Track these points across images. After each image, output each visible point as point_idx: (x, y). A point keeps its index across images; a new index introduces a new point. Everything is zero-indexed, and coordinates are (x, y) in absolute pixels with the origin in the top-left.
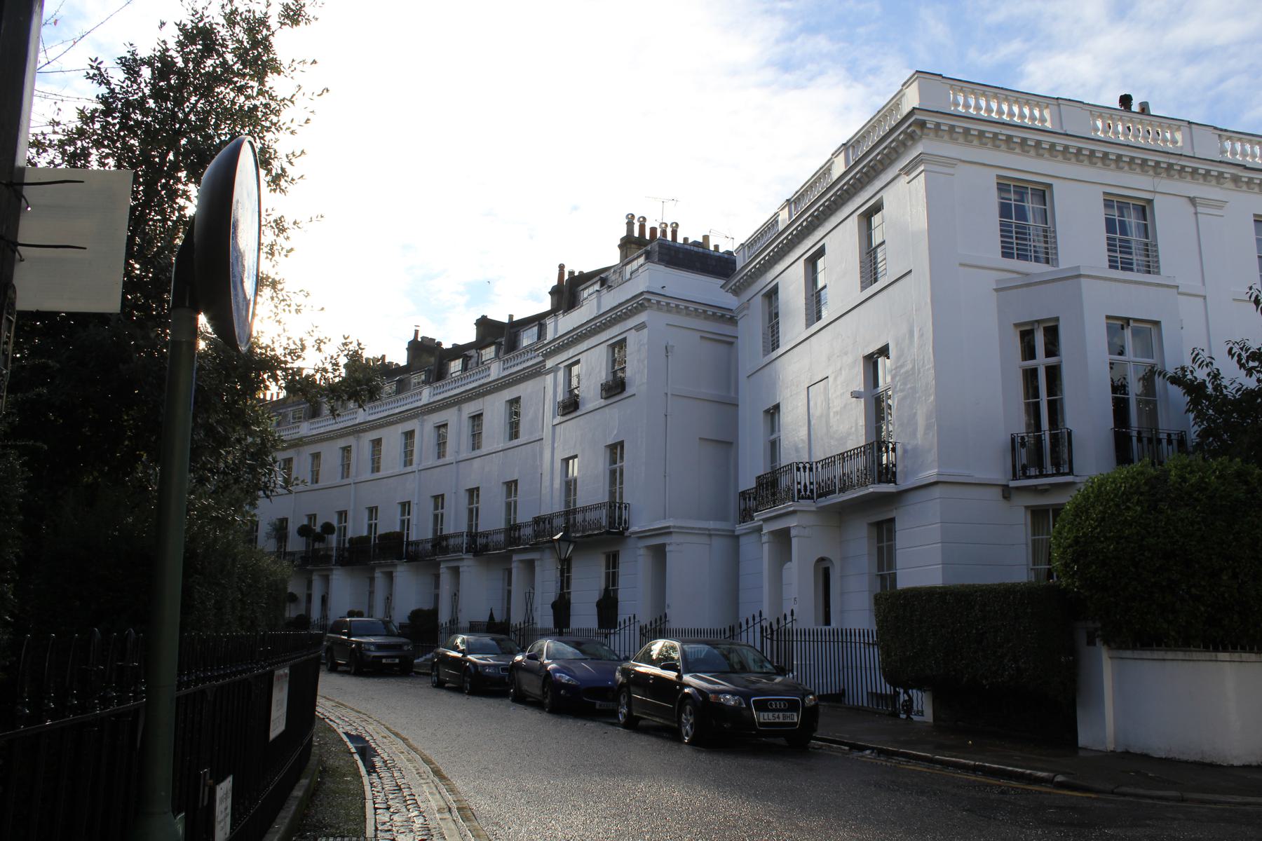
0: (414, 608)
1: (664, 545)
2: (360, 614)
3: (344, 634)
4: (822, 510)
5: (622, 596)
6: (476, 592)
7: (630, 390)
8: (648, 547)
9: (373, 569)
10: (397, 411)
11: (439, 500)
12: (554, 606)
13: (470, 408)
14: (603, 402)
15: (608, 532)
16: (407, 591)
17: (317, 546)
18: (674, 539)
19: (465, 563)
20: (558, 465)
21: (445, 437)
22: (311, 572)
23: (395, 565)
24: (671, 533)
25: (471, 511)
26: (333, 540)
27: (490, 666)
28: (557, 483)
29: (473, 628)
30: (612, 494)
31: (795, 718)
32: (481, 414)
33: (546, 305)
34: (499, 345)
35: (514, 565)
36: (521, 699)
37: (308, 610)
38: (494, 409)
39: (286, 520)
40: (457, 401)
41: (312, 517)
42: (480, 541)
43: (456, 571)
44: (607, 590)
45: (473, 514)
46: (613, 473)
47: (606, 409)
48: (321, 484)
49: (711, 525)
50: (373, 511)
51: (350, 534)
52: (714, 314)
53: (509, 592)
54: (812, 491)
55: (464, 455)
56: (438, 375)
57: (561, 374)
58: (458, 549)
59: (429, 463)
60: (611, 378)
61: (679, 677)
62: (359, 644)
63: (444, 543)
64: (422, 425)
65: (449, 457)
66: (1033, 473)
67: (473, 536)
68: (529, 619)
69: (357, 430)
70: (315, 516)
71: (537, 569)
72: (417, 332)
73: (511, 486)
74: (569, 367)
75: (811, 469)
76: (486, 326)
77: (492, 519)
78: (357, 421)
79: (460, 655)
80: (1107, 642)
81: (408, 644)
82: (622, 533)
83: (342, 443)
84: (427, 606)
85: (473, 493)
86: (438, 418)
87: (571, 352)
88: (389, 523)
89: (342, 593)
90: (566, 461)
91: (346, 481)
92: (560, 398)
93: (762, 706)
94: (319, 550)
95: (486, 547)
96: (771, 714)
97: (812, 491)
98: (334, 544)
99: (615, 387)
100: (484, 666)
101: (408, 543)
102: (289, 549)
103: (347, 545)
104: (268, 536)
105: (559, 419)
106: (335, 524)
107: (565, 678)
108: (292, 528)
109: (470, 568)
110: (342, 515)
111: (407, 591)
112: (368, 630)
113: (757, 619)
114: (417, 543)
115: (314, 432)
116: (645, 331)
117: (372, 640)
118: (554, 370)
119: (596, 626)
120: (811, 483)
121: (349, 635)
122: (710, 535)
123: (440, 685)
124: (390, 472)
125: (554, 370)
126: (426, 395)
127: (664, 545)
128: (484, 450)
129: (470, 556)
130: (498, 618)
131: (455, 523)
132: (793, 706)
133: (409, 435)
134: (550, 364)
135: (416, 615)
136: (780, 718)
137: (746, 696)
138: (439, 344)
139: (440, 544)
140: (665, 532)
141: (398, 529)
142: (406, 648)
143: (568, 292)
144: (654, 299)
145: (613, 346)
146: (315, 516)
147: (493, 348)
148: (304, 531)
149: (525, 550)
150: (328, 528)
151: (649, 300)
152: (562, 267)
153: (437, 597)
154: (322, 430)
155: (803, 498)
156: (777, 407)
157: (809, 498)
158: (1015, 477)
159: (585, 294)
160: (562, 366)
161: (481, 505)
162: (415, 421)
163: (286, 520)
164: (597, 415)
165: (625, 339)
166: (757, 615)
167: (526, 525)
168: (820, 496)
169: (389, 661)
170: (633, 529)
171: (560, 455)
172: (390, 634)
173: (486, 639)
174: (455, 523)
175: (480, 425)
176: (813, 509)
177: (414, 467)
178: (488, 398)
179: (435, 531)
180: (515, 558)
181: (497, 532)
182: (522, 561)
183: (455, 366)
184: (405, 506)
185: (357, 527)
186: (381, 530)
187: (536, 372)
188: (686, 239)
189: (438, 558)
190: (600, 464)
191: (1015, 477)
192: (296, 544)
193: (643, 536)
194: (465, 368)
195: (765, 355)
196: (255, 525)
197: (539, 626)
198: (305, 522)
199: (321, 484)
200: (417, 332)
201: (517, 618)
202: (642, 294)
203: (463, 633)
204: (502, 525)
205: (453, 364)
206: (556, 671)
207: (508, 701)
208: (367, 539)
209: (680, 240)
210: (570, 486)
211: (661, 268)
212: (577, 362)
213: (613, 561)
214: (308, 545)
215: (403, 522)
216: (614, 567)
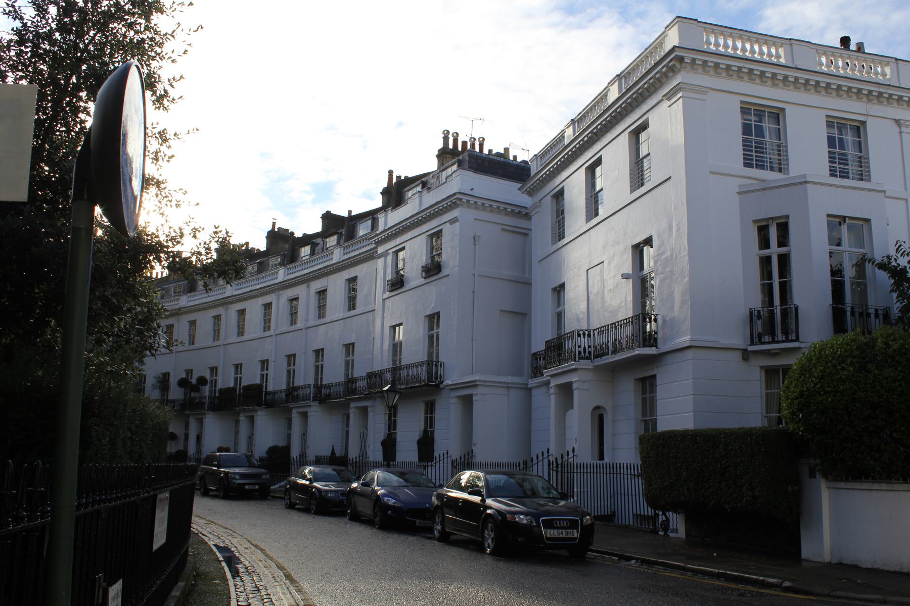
0: (271, 444)
1: (471, 396)
2: (227, 450)
3: (215, 466)
4: (598, 368)
5: (437, 436)
6: (321, 431)
7: (445, 272)
8: (458, 397)
9: (238, 414)
10: (258, 287)
11: (291, 358)
13: (317, 285)
14: (423, 281)
15: (427, 385)
16: (266, 432)
17: (193, 395)
18: (479, 390)
19: (312, 409)
20: (387, 331)
22: (188, 416)
23: (256, 411)
24: (477, 386)
25: (317, 367)
26: (206, 390)
27: (331, 491)
28: (387, 345)
29: (318, 461)
30: (430, 354)
31: (576, 534)
32: (326, 290)
33: (378, 203)
34: (340, 235)
35: (351, 411)
36: (356, 518)
37: (186, 445)
38: (336, 285)
39: (169, 374)
41: (189, 372)
42: (325, 391)
43: (305, 416)
44: (425, 431)
48: (196, 346)
49: (509, 379)
50: (238, 367)
51: (220, 386)
52: (513, 211)
53: (347, 432)
54: (590, 353)
55: (312, 322)
56: (291, 258)
57: (390, 258)
58: (306, 398)
60: (429, 261)
61: (483, 501)
62: (226, 474)
63: (296, 393)
64: (278, 299)
65: (300, 324)
66: (780, 339)
67: (318, 387)
68: (363, 454)
69: (225, 302)
70: (191, 371)
71: (370, 414)
72: (274, 224)
73: (350, 348)
74: (396, 253)
75: (589, 336)
76: (328, 217)
77: (334, 374)
79: (308, 483)
80: (826, 476)
81: (266, 474)
82: (437, 386)
83: (214, 312)
84: (281, 443)
85: (319, 353)
87: (398, 240)
88: (251, 377)
89: (214, 433)
90: (393, 328)
91: (216, 343)
92: (389, 277)
93: (549, 525)
94: (194, 398)
95: (329, 396)
96: (556, 531)
97: (590, 353)
98: (207, 394)
99: (433, 269)
100: (327, 491)
102: (170, 398)
103: (217, 394)
104: (154, 387)
105: (388, 294)
106: (208, 377)
107: (391, 501)
108: (173, 381)
109: (316, 413)
110: (214, 370)
111: (266, 432)
112: (234, 463)
113: (546, 455)
114: (274, 393)
115: (191, 304)
116: (458, 224)
117: (237, 470)
118: (385, 254)
120: (589, 347)
121: (219, 466)
122: (508, 388)
123: (291, 506)
124: (252, 336)
125: (385, 254)
126: (282, 275)
127: (471, 396)
130: (338, 453)
132: (573, 525)
133: (268, 306)
134: (381, 250)
135: (273, 450)
136: (563, 534)
137: (536, 516)
138: (292, 233)
139: (292, 393)
140: (473, 385)
141: (258, 382)
142: (264, 477)
143: (396, 192)
144: (465, 198)
145: (431, 236)
146: (191, 371)
147: (335, 237)
148: (183, 383)
150: (202, 381)
151: (461, 199)
152: (391, 172)
153: (289, 436)
154: (198, 302)
155: (582, 358)
156: (562, 286)
157: (587, 358)
158: (752, 343)
159: (410, 194)
160: (390, 251)
161: (325, 363)
162: (273, 295)
163: (169, 374)
165: (441, 231)
166: (545, 452)
167: (361, 379)
168: (596, 357)
169: (251, 487)
170: (448, 382)
172: (252, 466)
173: (329, 470)
174: (304, 377)
175: (325, 299)
176: (591, 367)
177: (272, 332)
179: (288, 383)
180: (352, 405)
181: (337, 384)
184: (265, 364)
185: (225, 380)
186: (245, 383)
187: (370, 256)
188: (490, 151)
189: (291, 405)
190: (421, 330)
191: (752, 343)
192: (176, 393)
193: (455, 388)
194: (313, 253)
195: (553, 244)
196: (143, 378)
197: (371, 459)
198: (184, 376)
199: (196, 346)
200: (274, 224)
201: (353, 454)
202: (455, 194)
203: (310, 465)
204: (342, 379)
205: (303, 249)
206: (384, 495)
207: (346, 519)
208: (233, 390)
209: (486, 151)
210: (396, 348)
211: (471, 174)
212: (403, 249)
213: (430, 408)
214: (185, 394)
215: (262, 376)
216: (431, 413)
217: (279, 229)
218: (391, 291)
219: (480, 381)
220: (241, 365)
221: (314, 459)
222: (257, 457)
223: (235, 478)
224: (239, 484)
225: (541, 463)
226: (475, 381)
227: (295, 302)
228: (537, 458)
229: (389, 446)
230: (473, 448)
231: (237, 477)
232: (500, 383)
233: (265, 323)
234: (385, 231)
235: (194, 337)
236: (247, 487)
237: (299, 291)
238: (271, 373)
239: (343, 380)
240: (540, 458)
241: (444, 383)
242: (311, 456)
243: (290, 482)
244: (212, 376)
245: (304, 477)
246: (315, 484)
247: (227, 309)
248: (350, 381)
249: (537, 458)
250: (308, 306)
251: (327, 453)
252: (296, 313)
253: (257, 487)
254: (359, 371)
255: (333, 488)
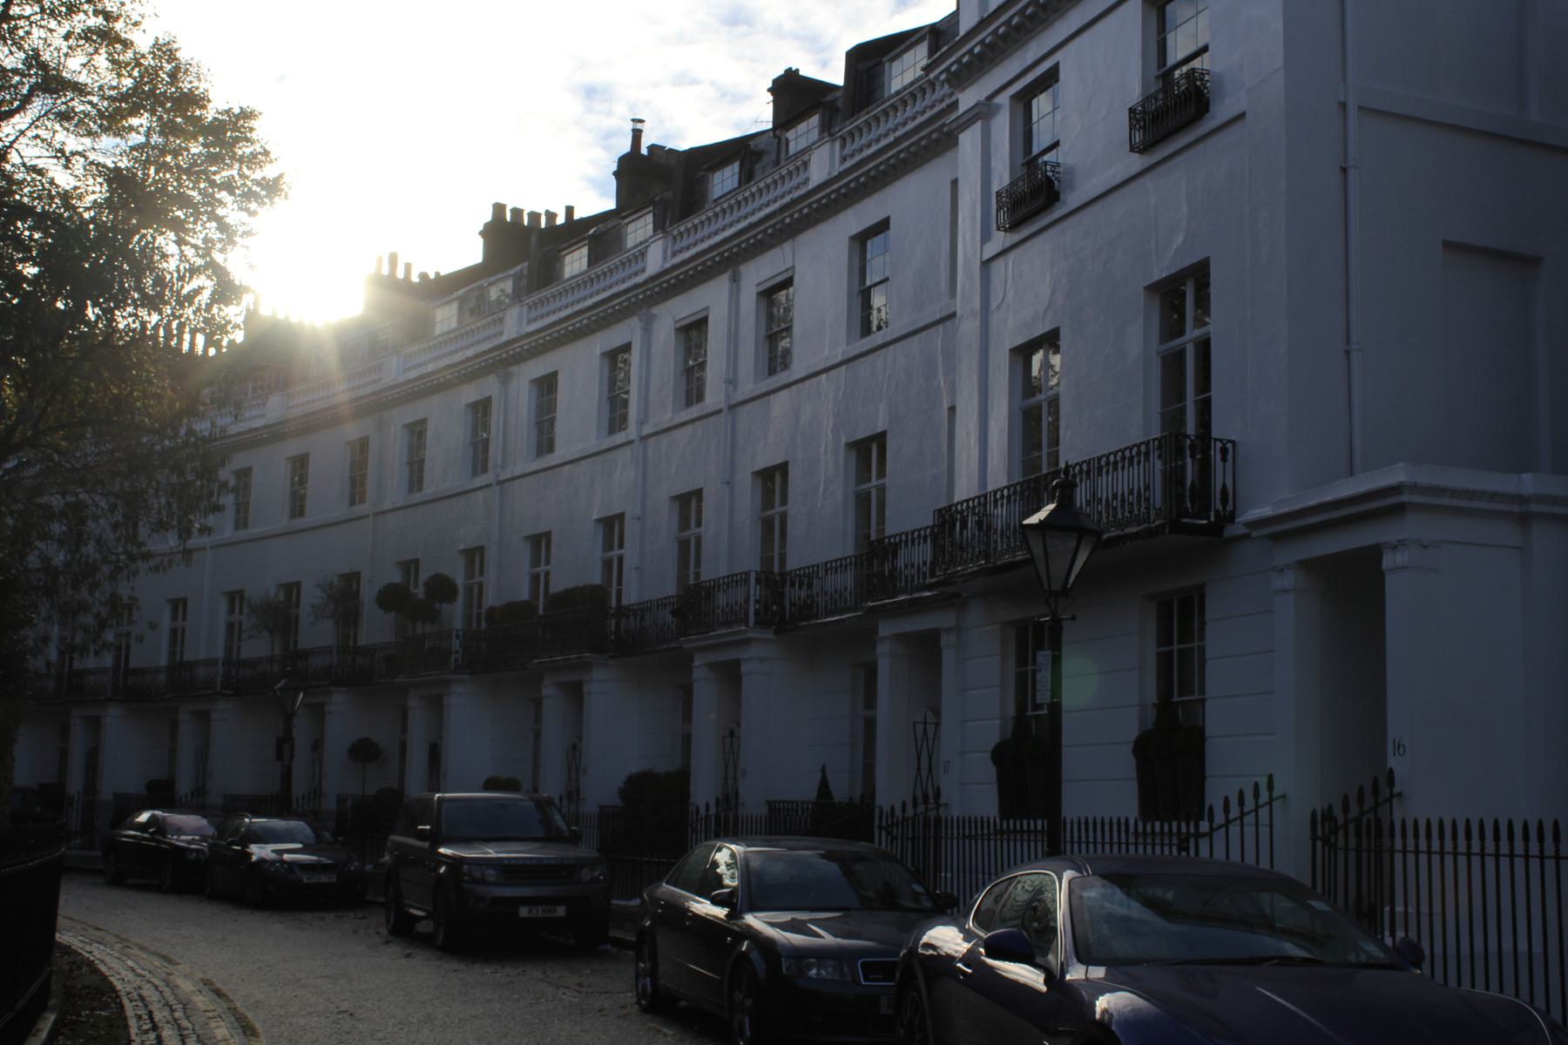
0: (635, 768)
1: (1372, 555)
5: (1218, 721)
7: (1221, 111)
8: (1308, 565)
12: (1144, 748)
13: (759, 272)
14: (1137, 162)
18: (1411, 528)
21: (701, 381)
25: (767, 525)
26: (455, 613)
27: (821, 954)
29: (778, 822)
30: (1172, 418)
35: (883, 649)
40: (726, 261)
42: (795, 594)
43: (730, 674)
44: (1165, 705)
45: (772, 530)
46: (1173, 365)
47: (1147, 181)
51: (491, 600)
53: (870, 725)
55: (747, 388)
57: (1002, 125)
59: (667, 417)
64: (647, 330)
67: (773, 580)
68: (928, 795)
70: (416, 562)
71: (948, 657)
72: (637, 135)
74: (1024, 99)
78: (504, 338)
79: (721, 912)
82: (1216, 530)
84: (662, 766)
85: (773, 479)
86: (682, 307)
88: (576, 566)
90: (1023, 353)
92: (1002, 178)
95: (807, 610)
98: (458, 624)
99: (1173, 110)
100: (799, 954)
101: (622, 611)
102: (363, 641)
103: (484, 625)
105: (1000, 240)
106: (460, 580)
108: (368, 593)
109: (766, 669)
110: (474, 556)
111: (617, 730)
114: (643, 609)
117: (491, 852)
118: (983, 112)
119: (1128, 807)
121: (437, 839)
122: (1524, 520)
124: (576, 450)
125: (983, 112)
127: (1372, 555)
128: (798, 368)
129: (769, 635)
130: (841, 790)
131: (729, 547)
134: (968, 99)
135: (637, 786)
139: (694, 604)
142: (586, 875)
146: (416, 562)
147: (815, 120)
148: (392, 598)
149: (916, 607)
150: (442, 588)
153: (687, 739)
164: (1119, 206)
167: (912, 538)
169: (538, 912)
171: (1009, 334)
172: (551, 836)
173: (808, 855)
177: (632, 432)
178: (806, 237)
180: (886, 629)
182: (901, 638)
183: (725, 180)
185: (507, 583)
186: (559, 584)
190: (1137, 339)
192: (376, 628)
193: (1288, 529)
197: (955, 812)
198: (397, 577)
199: (429, 490)
200: (637, 135)
201: (892, 792)
204: (846, 548)
208: (526, 608)
213: (1181, 621)
215: (607, 564)
216: (1185, 636)
217: (652, 148)
218: (1013, 227)
219: (1415, 488)
220: (548, 535)
221: (764, 811)
222: (590, 807)
223: (483, 881)
224: (498, 901)
225: (1249, 819)
226: (1396, 489)
227: (694, 334)
228: (1241, 802)
229: (1030, 764)
230: (1393, 762)
231: (491, 874)
232: (1493, 496)
233: (612, 410)
234: (983, 23)
235: (421, 470)
236: (524, 912)
237: (712, 297)
238: (631, 553)
239: (850, 551)
240: (1250, 803)
241: (1241, 519)
242: (753, 805)
243: (655, 900)
244: (470, 574)
245: (708, 884)
246: (753, 920)
247: (505, 380)
248: (875, 554)
249: (1241, 802)
250: (734, 338)
251: (807, 791)
252: (702, 366)
253: (561, 911)
254: (907, 513)
255: (828, 939)
